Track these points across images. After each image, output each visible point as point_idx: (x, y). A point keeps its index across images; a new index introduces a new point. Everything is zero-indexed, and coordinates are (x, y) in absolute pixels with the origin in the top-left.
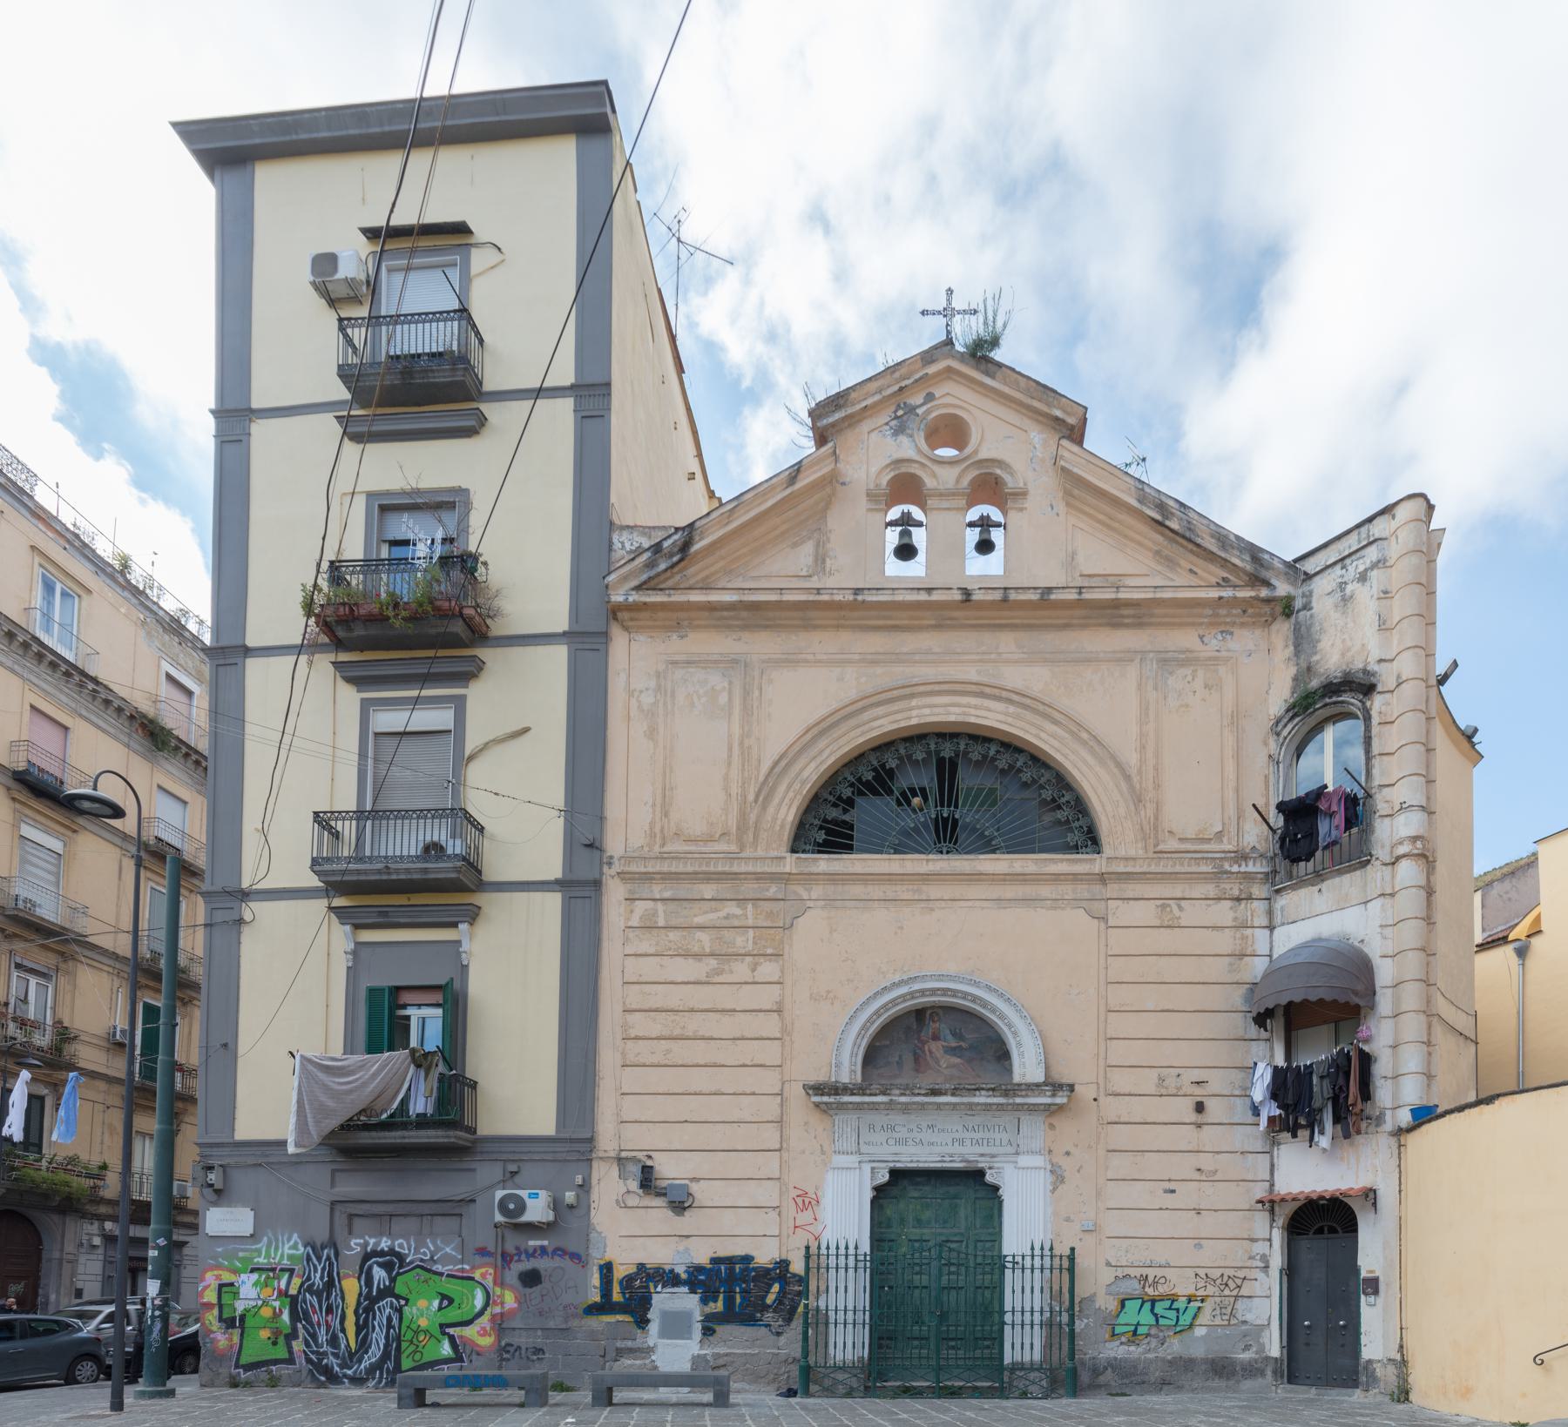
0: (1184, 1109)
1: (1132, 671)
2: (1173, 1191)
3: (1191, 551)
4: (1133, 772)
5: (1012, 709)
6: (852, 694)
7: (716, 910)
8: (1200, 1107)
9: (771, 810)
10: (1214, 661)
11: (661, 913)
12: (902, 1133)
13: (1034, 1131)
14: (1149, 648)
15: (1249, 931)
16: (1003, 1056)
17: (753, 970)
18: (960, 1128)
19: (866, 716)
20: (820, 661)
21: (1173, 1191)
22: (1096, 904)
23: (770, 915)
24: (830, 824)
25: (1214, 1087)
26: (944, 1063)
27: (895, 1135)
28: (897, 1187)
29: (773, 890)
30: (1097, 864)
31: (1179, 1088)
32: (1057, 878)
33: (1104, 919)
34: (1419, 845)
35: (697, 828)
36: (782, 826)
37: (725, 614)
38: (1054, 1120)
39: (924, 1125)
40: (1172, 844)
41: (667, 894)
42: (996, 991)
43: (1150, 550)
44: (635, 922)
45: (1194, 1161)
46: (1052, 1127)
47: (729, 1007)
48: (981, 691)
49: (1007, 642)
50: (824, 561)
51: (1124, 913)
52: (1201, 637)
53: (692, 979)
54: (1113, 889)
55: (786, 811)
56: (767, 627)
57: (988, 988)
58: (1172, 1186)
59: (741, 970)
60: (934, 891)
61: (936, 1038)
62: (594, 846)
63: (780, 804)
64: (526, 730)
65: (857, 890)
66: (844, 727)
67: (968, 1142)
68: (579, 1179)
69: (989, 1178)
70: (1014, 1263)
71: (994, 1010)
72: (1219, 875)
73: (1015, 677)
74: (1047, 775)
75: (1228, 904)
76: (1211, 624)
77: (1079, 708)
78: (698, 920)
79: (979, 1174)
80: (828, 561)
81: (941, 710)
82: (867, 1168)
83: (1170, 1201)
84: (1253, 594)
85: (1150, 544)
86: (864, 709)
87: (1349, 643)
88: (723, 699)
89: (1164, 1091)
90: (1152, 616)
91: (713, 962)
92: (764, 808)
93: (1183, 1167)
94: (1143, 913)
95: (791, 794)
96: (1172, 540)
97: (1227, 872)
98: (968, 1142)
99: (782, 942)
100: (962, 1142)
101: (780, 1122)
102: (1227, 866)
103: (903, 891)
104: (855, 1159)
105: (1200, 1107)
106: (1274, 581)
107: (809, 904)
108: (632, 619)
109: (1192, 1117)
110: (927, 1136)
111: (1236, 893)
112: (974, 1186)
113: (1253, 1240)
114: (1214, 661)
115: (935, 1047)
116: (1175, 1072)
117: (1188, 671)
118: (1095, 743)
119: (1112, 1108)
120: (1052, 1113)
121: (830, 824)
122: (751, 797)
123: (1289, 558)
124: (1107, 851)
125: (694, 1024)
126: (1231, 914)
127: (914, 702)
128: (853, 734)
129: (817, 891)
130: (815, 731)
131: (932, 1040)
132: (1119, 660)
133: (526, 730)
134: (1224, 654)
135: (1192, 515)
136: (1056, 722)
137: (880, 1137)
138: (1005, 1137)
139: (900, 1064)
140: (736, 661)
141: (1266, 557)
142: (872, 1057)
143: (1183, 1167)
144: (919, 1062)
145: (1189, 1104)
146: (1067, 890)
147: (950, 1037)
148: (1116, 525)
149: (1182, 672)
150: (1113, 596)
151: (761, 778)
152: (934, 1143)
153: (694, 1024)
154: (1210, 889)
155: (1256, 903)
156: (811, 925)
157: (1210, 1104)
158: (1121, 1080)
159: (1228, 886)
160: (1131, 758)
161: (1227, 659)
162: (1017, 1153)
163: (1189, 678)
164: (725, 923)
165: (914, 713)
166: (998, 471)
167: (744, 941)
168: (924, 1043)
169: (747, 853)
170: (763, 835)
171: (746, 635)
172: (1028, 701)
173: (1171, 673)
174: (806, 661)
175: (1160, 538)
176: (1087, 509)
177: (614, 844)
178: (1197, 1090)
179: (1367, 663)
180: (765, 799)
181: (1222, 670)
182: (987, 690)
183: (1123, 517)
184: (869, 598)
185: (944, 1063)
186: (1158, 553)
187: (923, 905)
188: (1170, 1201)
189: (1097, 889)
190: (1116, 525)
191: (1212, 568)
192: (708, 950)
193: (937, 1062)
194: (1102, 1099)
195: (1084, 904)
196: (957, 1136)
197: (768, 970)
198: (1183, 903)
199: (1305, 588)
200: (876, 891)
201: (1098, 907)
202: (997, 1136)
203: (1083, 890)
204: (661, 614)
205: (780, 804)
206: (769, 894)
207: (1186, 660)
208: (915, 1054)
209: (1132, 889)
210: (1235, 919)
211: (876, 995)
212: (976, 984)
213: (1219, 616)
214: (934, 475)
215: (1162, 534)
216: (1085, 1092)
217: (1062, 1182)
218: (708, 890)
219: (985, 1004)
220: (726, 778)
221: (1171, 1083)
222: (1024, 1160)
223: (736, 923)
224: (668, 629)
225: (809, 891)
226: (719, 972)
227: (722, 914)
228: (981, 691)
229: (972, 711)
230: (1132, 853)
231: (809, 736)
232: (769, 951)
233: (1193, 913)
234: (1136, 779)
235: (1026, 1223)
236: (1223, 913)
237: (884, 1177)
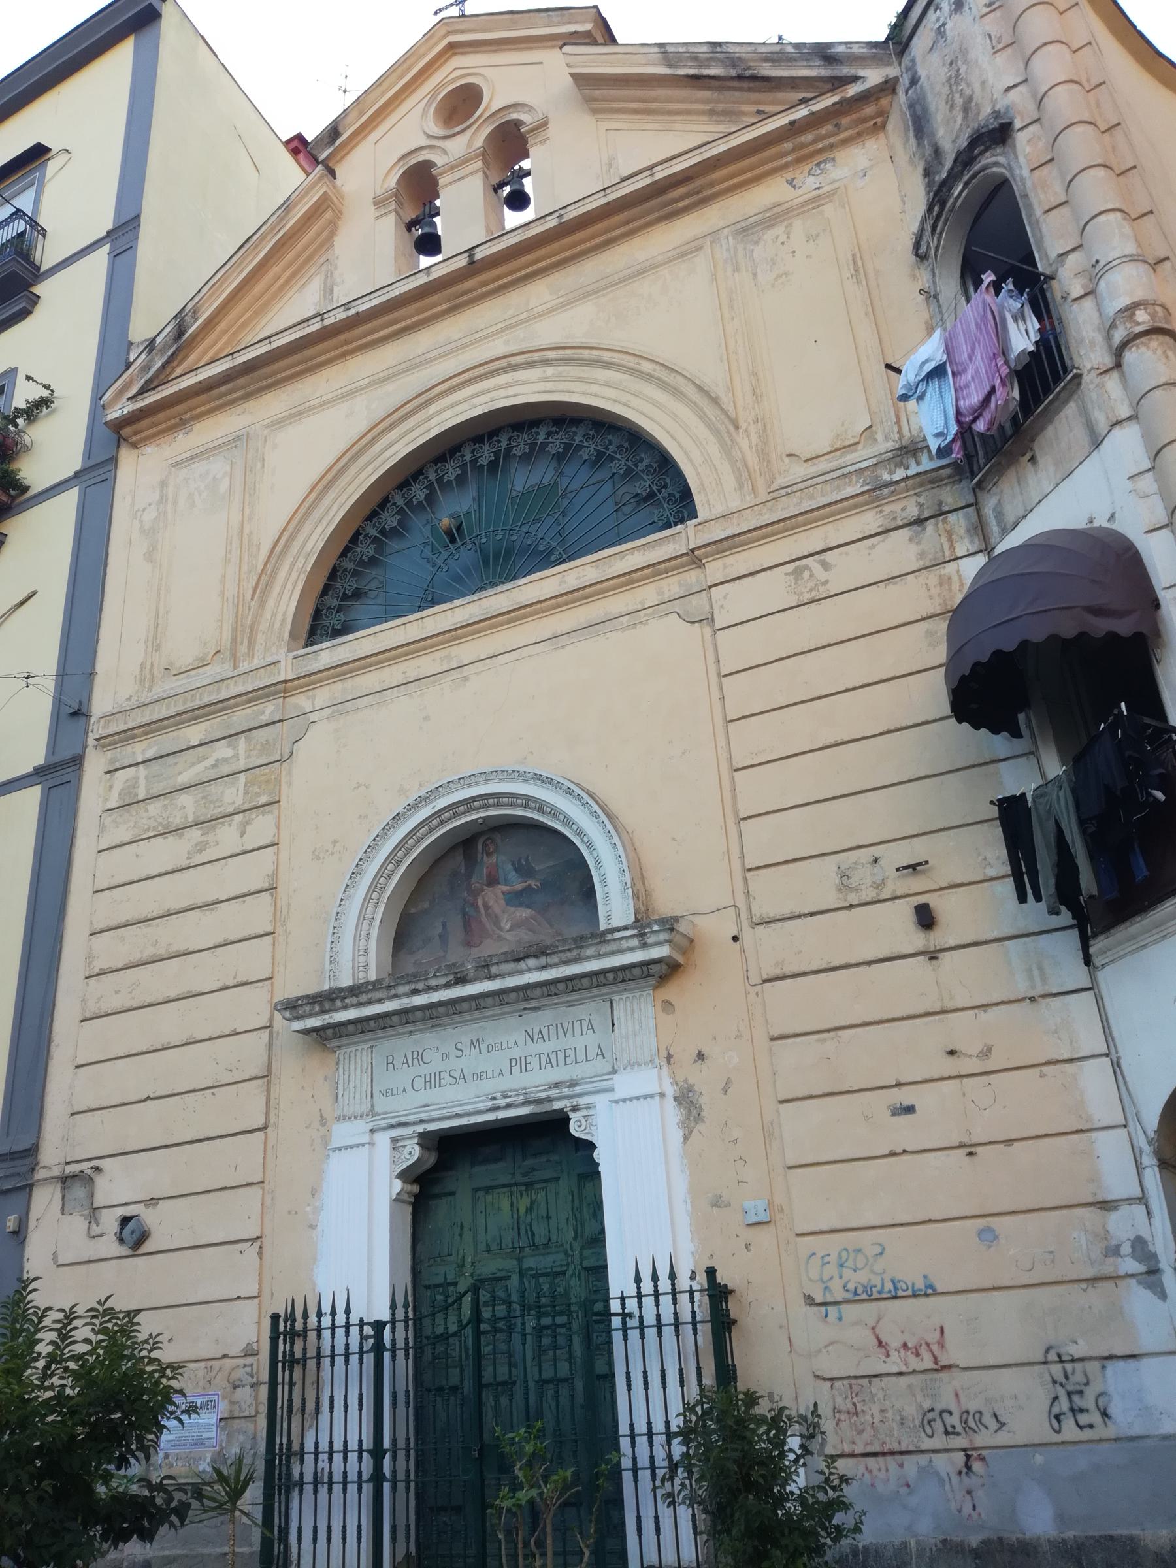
0: (894, 926)
1: (701, 262)
2: (910, 1109)
3: (749, 90)
4: (720, 391)
5: (550, 371)
6: (363, 426)
7: (205, 758)
8: (925, 918)
9: (271, 604)
10: (816, 202)
11: (142, 782)
12: (435, 1063)
13: (638, 1016)
14: (721, 224)
15: (951, 567)
16: (588, 893)
17: (243, 834)
18: (520, 1037)
19: (377, 447)
20: (327, 402)
21: (910, 1109)
22: (694, 600)
23: (267, 746)
24: (338, 600)
25: (944, 872)
26: (508, 921)
27: (425, 1070)
28: (449, 1165)
29: (269, 710)
30: (687, 536)
31: (879, 886)
32: (630, 579)
33: (710, 620)
34: (1141, 316)
35: (186, 659)
36: (284, 620)
37: (223, 389)
38: (670, 991)
39: (466, 1041)
40: (799, 471)
41: (150, 754)
42: (549, 780)
43: (703, 113)
44: (113, 804)
45: (931, 1036)
46: (668, 1006)
47: (210, 899)
48: (506, 364)
49: (539, 293)
50: (332, 291)
51: (734, 603)
52: (791, 183)
53: (170, 868)
54: (715, 569)
55: (287, 599)
56: (269, 387)
57: (539, 778)
58: (904, 1097)
59: (227, 837)
60: (466, 651)
61: (493, 881)
62: (80, 713)
63: (281, 594)
64: (33, 594)
65: (370, 680)
66: (352, 471)
67: (534, 1062)
68: (11, 1223)
69: (574, 1129)
70: (625, 1315)
71: (555, 813)
72: (876, 493)
73: (548, 332)
74: (616, 440)
75: (905, 533)
76: (799, 161)
77: (624, 336)
78: (183, 779)
79: (559, 1122)
80: (336, 289)
81: (465, 406)
82: (383, 1140)
83: (904, 1132)
84: (836, 98)
85: (700, 107)
86: (374, 440)
87: (968, 92)
88: (224, 486)
89: (853, 898)
90: (712, 184)
91: (195, 834)
92: (262, 604)
93: (916, 1051)
94: (774, 590)
95: (294, 575)
96: (720, 89)
97: (887, 485)
98: (534, 1062)
99: (278, 781)
100: (523, 1064)
101: (266, 1076)
102: (886, 477)
103: (427, 664)
104: (363, 1126)
105: (925, 918)
106: (861, 73)
107: (312, 717)
108: (136, 433)
109: (918, 940)
110: (470, 1061)
111: (913, 512)
112: (541, 1149)
113: (1106, 1205)
114: (816, 202)
115: (494, 897)
116: (865, 855)
117: (779, 230)
118: (664, 376)
119: (771, 948)
120: (663, 979)
121: (338, 600)
122: (248, 597)
123: (881, 35)
124: (702, 513)
125: (169, 935)
126: (914, 549)
127: (433, 409)
128: (363, 475)
129: (323, 695)
130: (320, 487)
131: (492, 882)
132: (683, 255)
133: (33, 594)
134: (826, 189)
135: (731, 49)
136: (607, 365)
137: (403, 1076)
138: (590, 1040)
139: (444, 938)
140: (239, 438)
141: (841, 49)
142: (404, 934)
143: (916, 1051)
144: (471, 929)
145: (904, 911)
146: (648, 593)
147: (513, 875)
148: (653, 106)
149: (769, 235)
150: (648, 181)
151: (260, 567)
152: (479, 1076)
153: (169, 935)
154: (870, 521)
155: (952, 518)
156: (318, 744)
157: (940, 904)
158: (772, 894)
159: (896, 507)
160: (713, 375)
161: (831, 195)
162: (614, 1072)
163: (783, 238)
164: (213, 774)
165: (433, 422)
166: (514, 116)
167: (232, 795)
168: (475, 893)
169: (244, 666)
170: (261, 639)
171: (250, 405)
172: (568, 353)
173: (757, 243)
174: (313, 408)
175: (707, 94)
176: (615, 105)
177: (102, 702)
178: (916, 884)
179: (994, 102)
180: (264, 591)
181: (828, 209)
182: (517, 360)
183: (661, 92)
184: (361, 308)
185: (508, 921)
186: (712, 113)
187: (455, 675)
188: (904, 1132)
189: (693, 577)
190: (653, 106)
191: (780, 95)
192: (191, 819)
193: (496, 921)
194: (747, 935)
195: (676, 606)
196: (517, 1053)
197: (261, 828)
198: (828, 556)
199: (906, 60)
200: (392, 674)
201: (698, 603)
202: (579, 1042)
203: (672, 586)
204: (161, 416)
205: (281, 594)
206: (264, 718)
207: (775, 216)
208: (464, 914)
209: (740, 562)
210: (922, 555)
211: (387, 829)
212: (521, 776)
213: (801, 144)
214: (445, 152)
215: (709, 88)
216: (715, 929)
217: (699, 1118)
218: (194, 733)
219: (541, 806)
220: (223, 581)
221: (864, 878)
222: (625, 1084)
223: (226, 770)
224: (174, 428)
225: (313, 698)
226: (201, 847)
227: (211, 761)
228: (506, 364)
229: (503, 393)
230: (735, 504)
231: (313, 495)
232: (263, 800)
233: (849, 567)
234: (725, 401)
235: (651, 1222)
236: (901, 551)
237: (412, 1152)
